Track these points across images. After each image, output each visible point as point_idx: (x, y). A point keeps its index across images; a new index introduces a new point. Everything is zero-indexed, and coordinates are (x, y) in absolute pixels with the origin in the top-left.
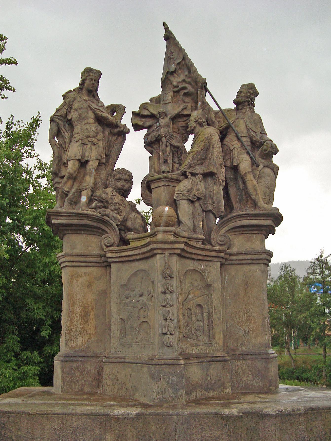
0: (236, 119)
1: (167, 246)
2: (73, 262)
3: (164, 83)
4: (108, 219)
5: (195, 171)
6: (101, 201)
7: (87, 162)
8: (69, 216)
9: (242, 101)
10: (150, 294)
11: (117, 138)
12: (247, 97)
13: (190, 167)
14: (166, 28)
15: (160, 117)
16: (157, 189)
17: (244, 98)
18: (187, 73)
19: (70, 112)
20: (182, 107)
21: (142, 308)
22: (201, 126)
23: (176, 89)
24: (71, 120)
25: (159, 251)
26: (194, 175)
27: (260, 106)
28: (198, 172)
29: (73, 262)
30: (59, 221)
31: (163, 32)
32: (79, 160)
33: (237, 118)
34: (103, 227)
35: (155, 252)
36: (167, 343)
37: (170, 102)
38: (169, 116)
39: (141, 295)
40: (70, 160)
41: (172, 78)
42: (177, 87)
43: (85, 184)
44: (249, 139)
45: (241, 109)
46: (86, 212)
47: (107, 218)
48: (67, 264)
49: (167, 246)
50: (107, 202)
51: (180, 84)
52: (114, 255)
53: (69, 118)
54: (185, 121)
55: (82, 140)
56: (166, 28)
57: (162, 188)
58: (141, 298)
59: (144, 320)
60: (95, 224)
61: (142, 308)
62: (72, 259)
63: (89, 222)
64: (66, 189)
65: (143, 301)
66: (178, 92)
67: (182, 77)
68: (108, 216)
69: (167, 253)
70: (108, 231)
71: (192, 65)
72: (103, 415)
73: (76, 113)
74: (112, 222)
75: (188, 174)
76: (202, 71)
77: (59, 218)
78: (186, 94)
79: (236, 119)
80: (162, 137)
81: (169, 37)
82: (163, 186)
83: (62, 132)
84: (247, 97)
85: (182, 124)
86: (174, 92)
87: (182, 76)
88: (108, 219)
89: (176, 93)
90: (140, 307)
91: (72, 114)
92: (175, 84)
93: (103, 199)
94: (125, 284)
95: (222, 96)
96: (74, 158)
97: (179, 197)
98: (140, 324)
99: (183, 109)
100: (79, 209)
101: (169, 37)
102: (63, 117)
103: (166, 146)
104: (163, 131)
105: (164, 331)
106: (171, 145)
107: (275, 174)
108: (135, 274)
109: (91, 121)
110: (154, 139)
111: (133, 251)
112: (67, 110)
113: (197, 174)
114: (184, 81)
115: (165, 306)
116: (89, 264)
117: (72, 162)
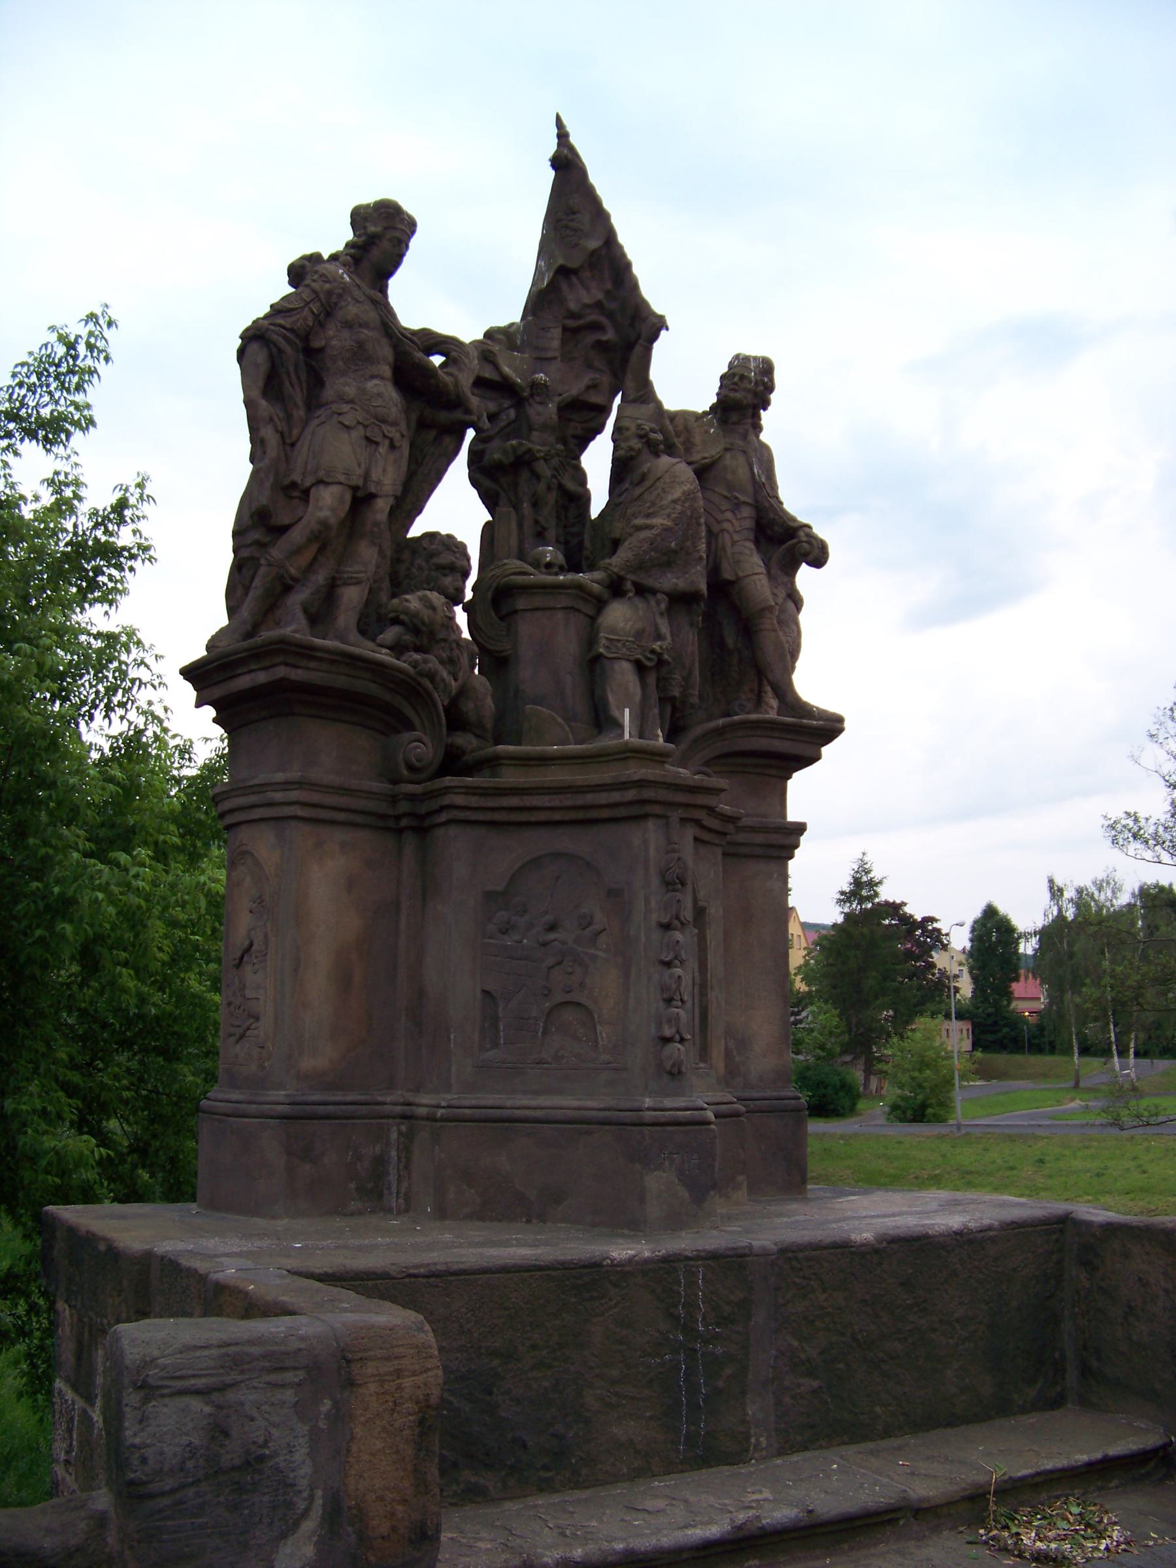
1: (681, 798)
2: (315, 806)
4: (430, 686)
5: (649, 582)
6: (416, 631)
7: (372, 497)
8: (333, 662)
9: (745, 402)
10: (590, 924)
11: (436, 439)
12: (747, 388)
13: (641, 566)
14: (563, 136)
15: (532, 395)
16: (539, 614)
18: (609, 286)
19: (322, 325)
20: (586, 380)
21: (560, 963)
22: (652, 452)
23: (571, 323)
24: (321, 350)
25: (657, 809)
26: (642, 591)
27: (775, 427)
28: (657, 586)
29: (315, 806)
30: (300, 671)
31: (552, 146)
32: (355, 489)
33: (728, 446)
34: (408, 711)
35: (648, 809)
36: (673, 1065)
37: (555, 358)
38: (557, 399)
39: (552, 928)
40: (327, 484)
41: (564, 287)
42: (573, 316)
43: (357, 568)
45: (734, 423)
46: (357, 651)
47: (426, 683)
48: (300, 811)
49: (681, 798)
50: (432, 635)
52: (474, 801)
53: (316, 344)
54: (586, 421)
55: (366, 427)
56: (563, 136)
58: (552, 936)
59: (568, 997)
60: (388, 697)
61: (560, 963)
62: (315, 797)
63: (374, 689)
64: (293, 571)
65: (564, 943)
66: (575, 331)
68: (432, 676)
69: (675, 815)
70: (417, 722)
71: (628, 266)
72: (584, 1267)
73: (346, 334)
74: (436, 695)
75: (628, 585)
76: (654, 290)
77: (304, 663)
78: (601, 346)
79: (726, 450)
80: (537, 459)
81: (567, 164)
82: (566, 608)
83: (287, 383)
84: (747, 388)
86: (565, 329)
87: (588, 287)
88: (430, 686)
89: (570, 333)
90: (550, 961)
91: (331, 333)
92: (573, 306)
93: (423, 623)
94: (500, 888)
95: (684, 379)
96: (342, 479)
98: (551, 1011)
99: (588, 388)
100: (759, 701)
101: (567, 164)
102: (298, 336)
103: (549, 488)
105: (668, 1032)
106: (561, 487)
108: (535, 863)
109: (387, 371)
110: (512, 459)
111: (547, 798)
112: (316, 316)
113: (653, 592)
114: (599, 305)
115: (668, 964)
116: (341, 816)
117: (335, 489)
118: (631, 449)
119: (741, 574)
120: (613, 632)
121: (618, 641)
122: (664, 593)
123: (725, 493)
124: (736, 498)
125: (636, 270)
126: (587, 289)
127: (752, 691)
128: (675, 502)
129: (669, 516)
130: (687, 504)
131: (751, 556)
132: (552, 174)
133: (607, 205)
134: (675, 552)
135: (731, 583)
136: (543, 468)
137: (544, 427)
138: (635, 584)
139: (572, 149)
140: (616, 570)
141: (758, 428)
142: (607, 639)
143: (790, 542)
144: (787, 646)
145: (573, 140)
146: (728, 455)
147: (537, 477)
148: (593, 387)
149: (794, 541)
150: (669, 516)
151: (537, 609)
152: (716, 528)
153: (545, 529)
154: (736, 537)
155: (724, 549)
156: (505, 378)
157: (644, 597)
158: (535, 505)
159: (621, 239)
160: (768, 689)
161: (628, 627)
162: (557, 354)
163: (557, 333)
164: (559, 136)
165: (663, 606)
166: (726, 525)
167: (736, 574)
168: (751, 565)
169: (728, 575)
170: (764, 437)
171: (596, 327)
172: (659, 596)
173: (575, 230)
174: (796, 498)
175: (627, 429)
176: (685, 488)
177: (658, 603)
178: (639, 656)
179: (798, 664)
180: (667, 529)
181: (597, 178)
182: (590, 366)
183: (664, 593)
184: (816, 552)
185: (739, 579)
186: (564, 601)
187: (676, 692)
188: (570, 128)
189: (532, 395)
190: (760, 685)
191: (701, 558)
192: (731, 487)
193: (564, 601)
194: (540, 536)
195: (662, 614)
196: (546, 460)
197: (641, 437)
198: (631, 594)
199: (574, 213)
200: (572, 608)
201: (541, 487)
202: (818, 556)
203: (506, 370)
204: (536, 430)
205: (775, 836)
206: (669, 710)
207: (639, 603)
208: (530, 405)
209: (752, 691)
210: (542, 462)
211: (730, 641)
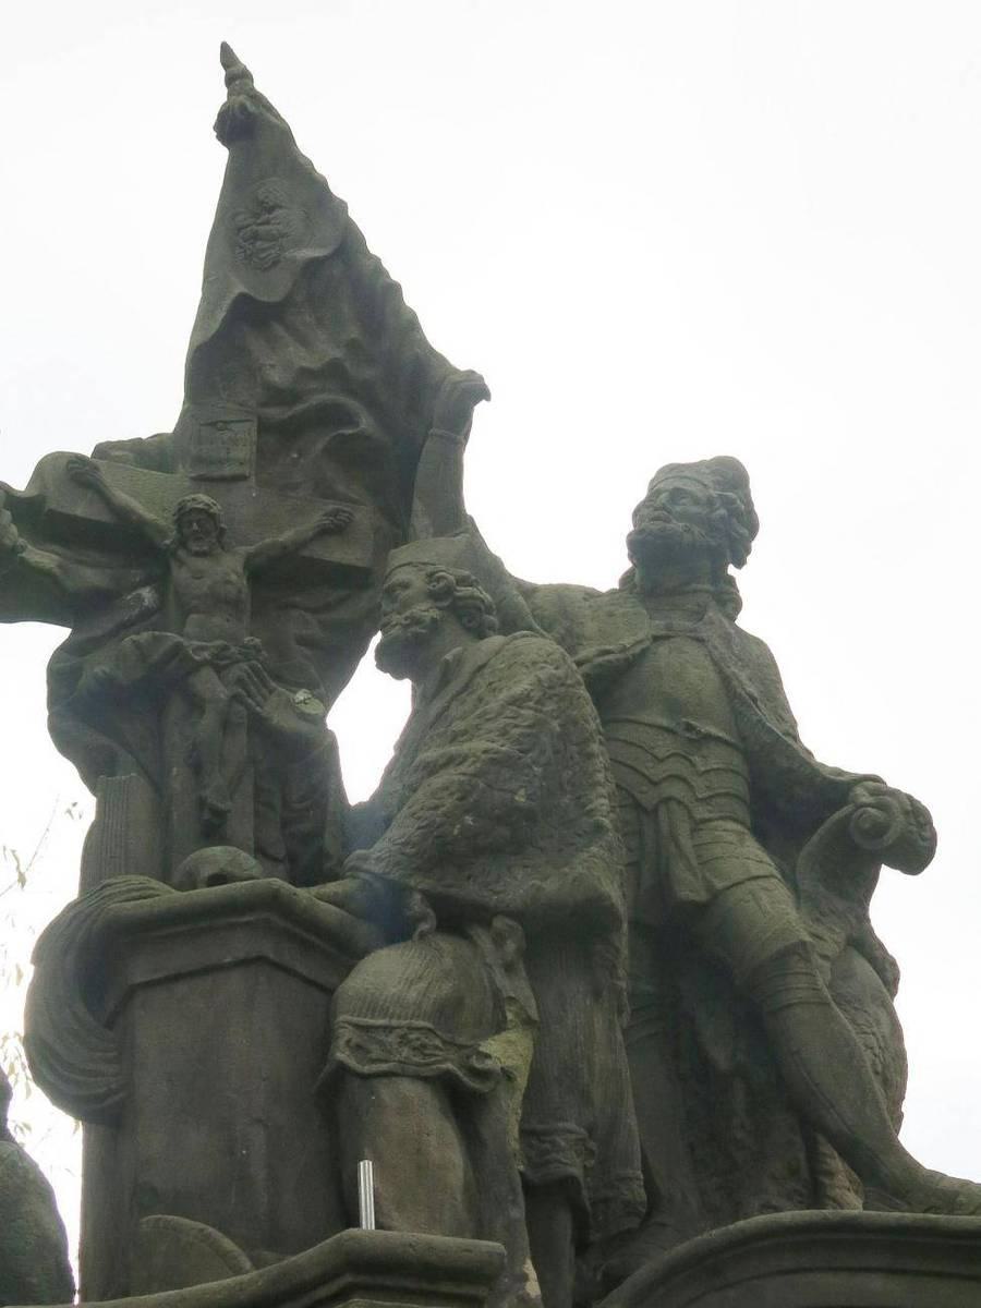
0: (656, 639)
3: (213, 364)
5: (470, 890)
12: (695, 533)
14: (237, 76)
16: (181, 988)
17: (696, 530)
18: (353, 332)
20: (316, 518)
23: (276, 413)
27: (769, 598)
31: (218, 95)
37: (243, 478)
38: (243, 550)
41: (256, 345)
42: (279, 396)
44: (737, 761)
51: (313, 385)
57: (235, 982)
67: (327, 350)
76: (451, 328)
80: (199, 666)
81: (248, 125)
84: (695, 533)
85: (314, 606)
86: (264, 427)
92: (276, 377)
95: (546, 509)
97: (376, 1052)
99: (323, 533)
103: (226, 725)
104: (195, 637)
107: (404, 1076)
114: (334, 371)
118: (416, 621)
119: (719, 885)
120: (373, 1008)
121: (388, 1029)
122: (510, 914)
123: (665, 722)
124: (689, 728)
125: (411, 299)
126: (304, 341)
127: (794, 1172)
128: (518, 701)
129: (504, 733)
130: (550, 707)
131: (742, 842)
132: (220, 155)
133: (337, 188)
134: (530, 816)
135: (701, 909)
136: (209, 685)
137: (218, 601)
138: (432, 898)
139: (258, 99)
140: (378, 869)
141: (729, 601)
142: (357, 1026)
143: (838, 815)
144: (868, 1056)
145: (260, 85)
146: (663, 649)
147: (196, 705)
148: (335, 529)
149: (846, 810)
150: (504, 733)
151: (177, 978)
152: (648, 797)
153: (221, 815)
154: (701, 812)
155: (674, 838)
156: (123, 514)
157: (465, 936)
158: (197, 768)
159: (376, 244)
160: (837, 1164)
161: (413, 995)
162: (246, 470)
163: (246, 432)
164: (230, 81)
165: (511, 946)
166: (676, 790)
167: (709, 887)
168: (759, 888)
169: (689, 889)
170: (746, 621)
171: (332, 416)
172: (500, 923)
173: (274, 238)
174: (835, 731)
175: (405, 586)
176: (542, 675)
177: (499, 941)
178: (449, 1066)
179: (906, 1107)
180: (498, 762)
181: (311, 143)
182: (324, 491)
183: (510, 914)
184: (899, 823)
185: (716, 895)
186: (241, 946)
187: (573, 1165)
188: (245, 57)
189: (182, 543)
190: (813, 1156)
191: (599, 828)
192: (674, 707)
193: (241, 946)
194: (213, 830)
195: (509, 968)
196: (219, 670)
197: (434, 596)
198: (424, 927)
199: (271, 210)
200: (260, 960)
201: (208, 722)
202: (906, 837)
203: (122, 497)
204: (196, 610)
205: (99, 632)
206: (564, 1225)
207: (446, 944)
208: (182, 563)
209: (794, 1172)
210: (207, 674)
211: (721, 1057)
